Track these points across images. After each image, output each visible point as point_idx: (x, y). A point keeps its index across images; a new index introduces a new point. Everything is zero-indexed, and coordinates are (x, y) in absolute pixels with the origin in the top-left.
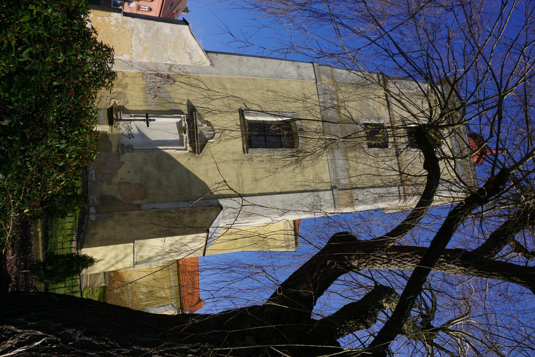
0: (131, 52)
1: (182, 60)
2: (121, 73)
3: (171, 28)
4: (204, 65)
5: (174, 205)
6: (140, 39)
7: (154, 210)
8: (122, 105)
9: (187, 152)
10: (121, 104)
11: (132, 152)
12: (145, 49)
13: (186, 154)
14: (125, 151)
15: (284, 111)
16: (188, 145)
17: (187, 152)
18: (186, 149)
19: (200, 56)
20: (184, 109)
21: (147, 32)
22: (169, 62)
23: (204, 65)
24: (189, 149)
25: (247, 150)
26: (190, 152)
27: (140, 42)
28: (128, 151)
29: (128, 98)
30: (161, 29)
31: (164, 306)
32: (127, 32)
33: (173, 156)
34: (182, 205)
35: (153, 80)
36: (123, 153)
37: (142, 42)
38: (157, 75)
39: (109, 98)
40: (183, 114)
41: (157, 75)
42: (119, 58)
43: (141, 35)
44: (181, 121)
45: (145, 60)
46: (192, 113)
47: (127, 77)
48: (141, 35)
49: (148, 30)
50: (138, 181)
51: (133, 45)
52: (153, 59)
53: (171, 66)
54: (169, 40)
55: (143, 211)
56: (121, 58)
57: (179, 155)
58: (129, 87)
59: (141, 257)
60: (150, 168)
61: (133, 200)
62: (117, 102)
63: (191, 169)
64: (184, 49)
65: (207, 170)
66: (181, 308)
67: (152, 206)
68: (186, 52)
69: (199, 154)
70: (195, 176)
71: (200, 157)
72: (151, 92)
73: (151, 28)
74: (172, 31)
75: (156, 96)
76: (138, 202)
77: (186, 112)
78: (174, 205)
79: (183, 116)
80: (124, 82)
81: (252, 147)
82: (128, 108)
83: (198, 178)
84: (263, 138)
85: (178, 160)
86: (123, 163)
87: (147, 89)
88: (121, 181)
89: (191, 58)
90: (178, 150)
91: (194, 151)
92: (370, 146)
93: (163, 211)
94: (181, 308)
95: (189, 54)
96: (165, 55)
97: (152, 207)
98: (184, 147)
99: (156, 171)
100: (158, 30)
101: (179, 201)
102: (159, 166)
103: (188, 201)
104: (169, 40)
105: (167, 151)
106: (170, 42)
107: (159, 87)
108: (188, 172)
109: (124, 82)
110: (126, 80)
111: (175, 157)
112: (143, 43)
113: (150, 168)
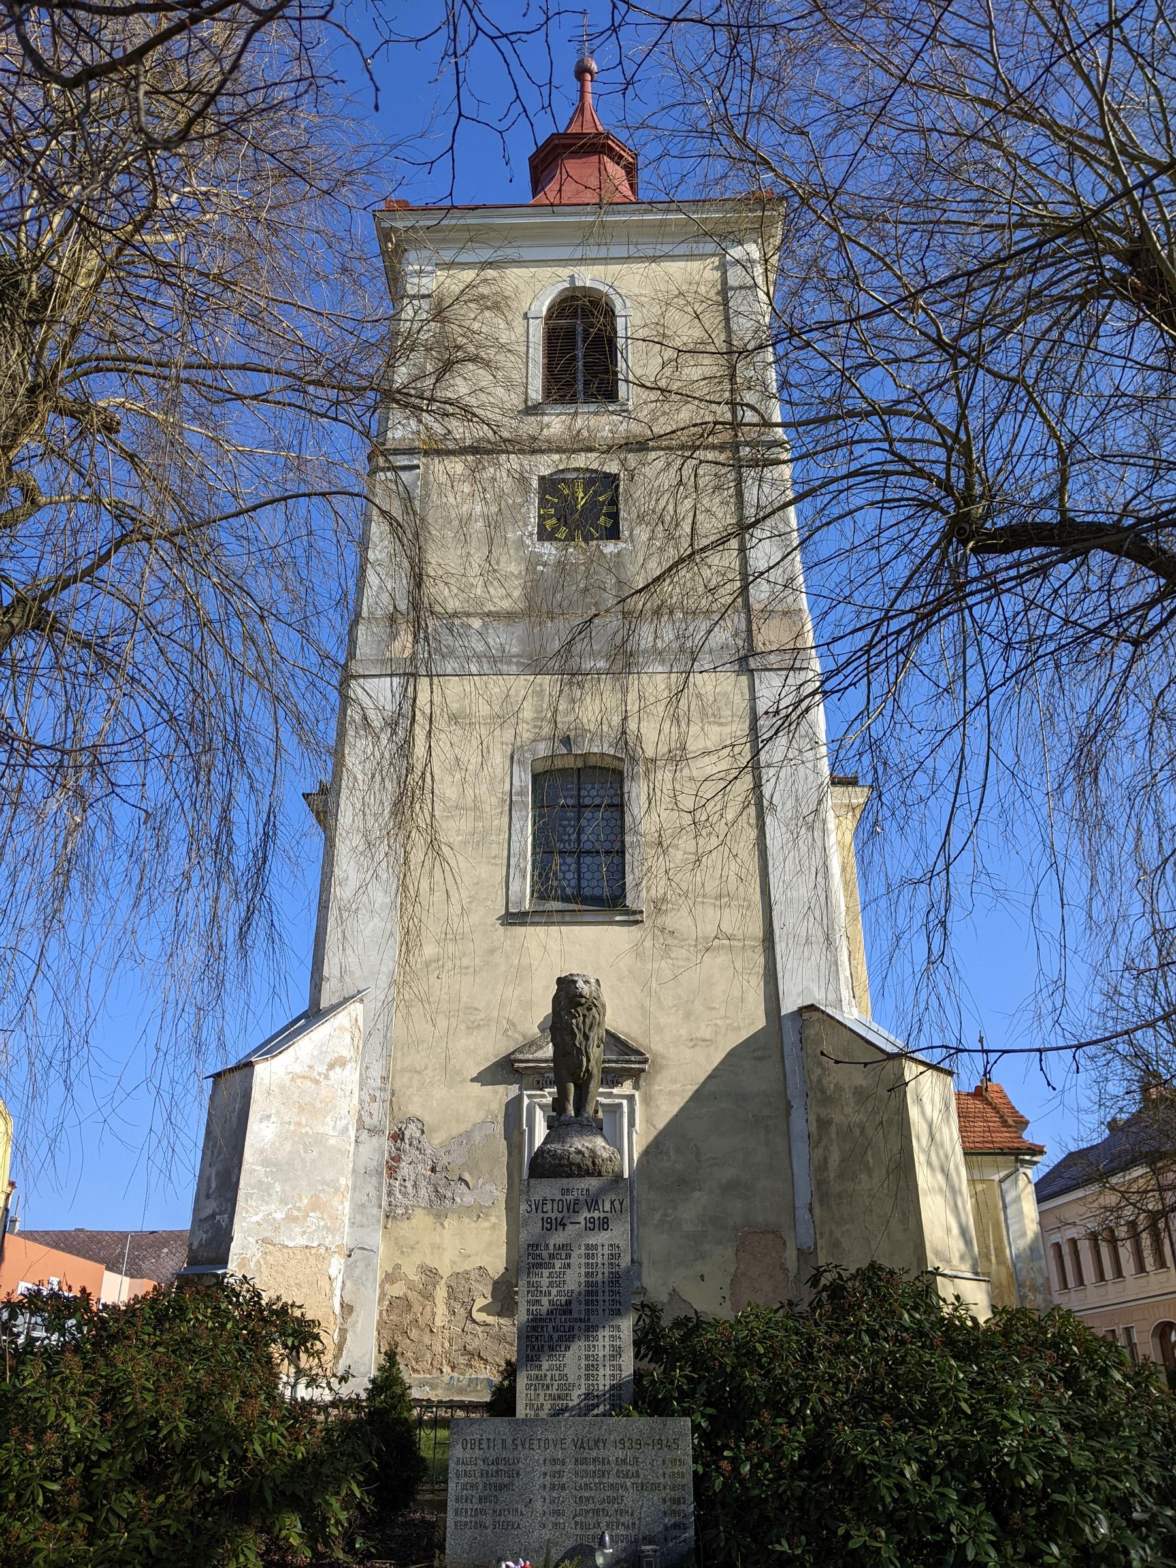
0: (322, 1250)
1: (346, 1092)
2: (387, 1286)
3: (261, 1120)
4: (361, 1023)
5: (800, 1149)
6: (290, 1218)
7: (817, 1211)
8: (490, 1288)
9: (637, 1094)
10: (488, 1290)
11: (640, 1264)
12: (315, 1206)
13: (647, 1101)
14: (637, 1284)
15: (507, 787)
16: (615, 1091)
17: (637, 1094)
18: (631, 1099)
19: (332, 1036)
20: (504, 1093)
21: (270, 1195)
22: (352, 1133)
23: (361, 1023)
24: (627, 1088)
25: (634, 913)
26: (636, 1087)
27: (295, 1219)
28: (639, 1278)
29: (467, 1266)
30: (262, 1151)
31: (1005, 1207)
32: (270, 1259)
33: (651, 1138)
34: (800, 1122)
35: (409, 1184)
36: (644, 1290)
37: (295, 1213)
38: (392, 1171)
39: (470, 1326)
40: (519, 1099)
41: (392, 1171)
42: (338, 1292)
43: (279, 1216)
44: (541, 1106)
45: (345, 1208)
46: (517, 1071)
47: (397, 1267)
48: (279, 1216)
49: (265, 1191)
50: (730, 1252)
51: (305, 1242)
52: (343, 1181)
53: (361, 1125)
54: (292, 1127)
55: (820, 1243)
56: (339, 1284)
57: (649, 1121)
58: (432, 1262)
59: (962, 1258)
60: (690, 1211)
61: (786, 1270)
62: (480, 1302)
63: (691, 1089)
64: (317, 1082)
65: (694, 1042)
66: (1017, 1155)
67: (803, 1214)
68: (327, 1077)
69: (645, 1061)
70: (710, 1077)
71: (655, 1055)
72: (449, 1194)
73: (260, 1182)
74: (269, 1117)
75: (460, 1179)
76: (791, 1254)
77: (514, 1090)
78: (800, 1149)
79: (526, 1101)
80: (416, 1278)
81: (623, 896)
82: (502, 1271)
83: (716, 1069)
84: (588, 860)
85: (661, 1124)
86: (674, 1293)
87: (439, 1204)
88: (728, 1304)
89: (341, 1062)
90: (632, 1124)
91: (635, 1075)
92: (613, 533)
93: (819, 1183)
94: (1017, 1155)
95: (331, 1067)
96: (332, 1142)
97: (807, 1216)
98: (625, 1102)
99: (697, 1194)
100: (265, 1162)
101: (788, 1134)
102: (683, 1184)
103: (789, 1106)
104: (292, 1127)
105: (636, 1158)
106: (299, 1124)
107: (433, 1170)
108: (697, 1097)
109: (416, 1278)
110: (410, 1271)
111: (654, 1133)
112: (299, 1209)
113: (690, 1211)
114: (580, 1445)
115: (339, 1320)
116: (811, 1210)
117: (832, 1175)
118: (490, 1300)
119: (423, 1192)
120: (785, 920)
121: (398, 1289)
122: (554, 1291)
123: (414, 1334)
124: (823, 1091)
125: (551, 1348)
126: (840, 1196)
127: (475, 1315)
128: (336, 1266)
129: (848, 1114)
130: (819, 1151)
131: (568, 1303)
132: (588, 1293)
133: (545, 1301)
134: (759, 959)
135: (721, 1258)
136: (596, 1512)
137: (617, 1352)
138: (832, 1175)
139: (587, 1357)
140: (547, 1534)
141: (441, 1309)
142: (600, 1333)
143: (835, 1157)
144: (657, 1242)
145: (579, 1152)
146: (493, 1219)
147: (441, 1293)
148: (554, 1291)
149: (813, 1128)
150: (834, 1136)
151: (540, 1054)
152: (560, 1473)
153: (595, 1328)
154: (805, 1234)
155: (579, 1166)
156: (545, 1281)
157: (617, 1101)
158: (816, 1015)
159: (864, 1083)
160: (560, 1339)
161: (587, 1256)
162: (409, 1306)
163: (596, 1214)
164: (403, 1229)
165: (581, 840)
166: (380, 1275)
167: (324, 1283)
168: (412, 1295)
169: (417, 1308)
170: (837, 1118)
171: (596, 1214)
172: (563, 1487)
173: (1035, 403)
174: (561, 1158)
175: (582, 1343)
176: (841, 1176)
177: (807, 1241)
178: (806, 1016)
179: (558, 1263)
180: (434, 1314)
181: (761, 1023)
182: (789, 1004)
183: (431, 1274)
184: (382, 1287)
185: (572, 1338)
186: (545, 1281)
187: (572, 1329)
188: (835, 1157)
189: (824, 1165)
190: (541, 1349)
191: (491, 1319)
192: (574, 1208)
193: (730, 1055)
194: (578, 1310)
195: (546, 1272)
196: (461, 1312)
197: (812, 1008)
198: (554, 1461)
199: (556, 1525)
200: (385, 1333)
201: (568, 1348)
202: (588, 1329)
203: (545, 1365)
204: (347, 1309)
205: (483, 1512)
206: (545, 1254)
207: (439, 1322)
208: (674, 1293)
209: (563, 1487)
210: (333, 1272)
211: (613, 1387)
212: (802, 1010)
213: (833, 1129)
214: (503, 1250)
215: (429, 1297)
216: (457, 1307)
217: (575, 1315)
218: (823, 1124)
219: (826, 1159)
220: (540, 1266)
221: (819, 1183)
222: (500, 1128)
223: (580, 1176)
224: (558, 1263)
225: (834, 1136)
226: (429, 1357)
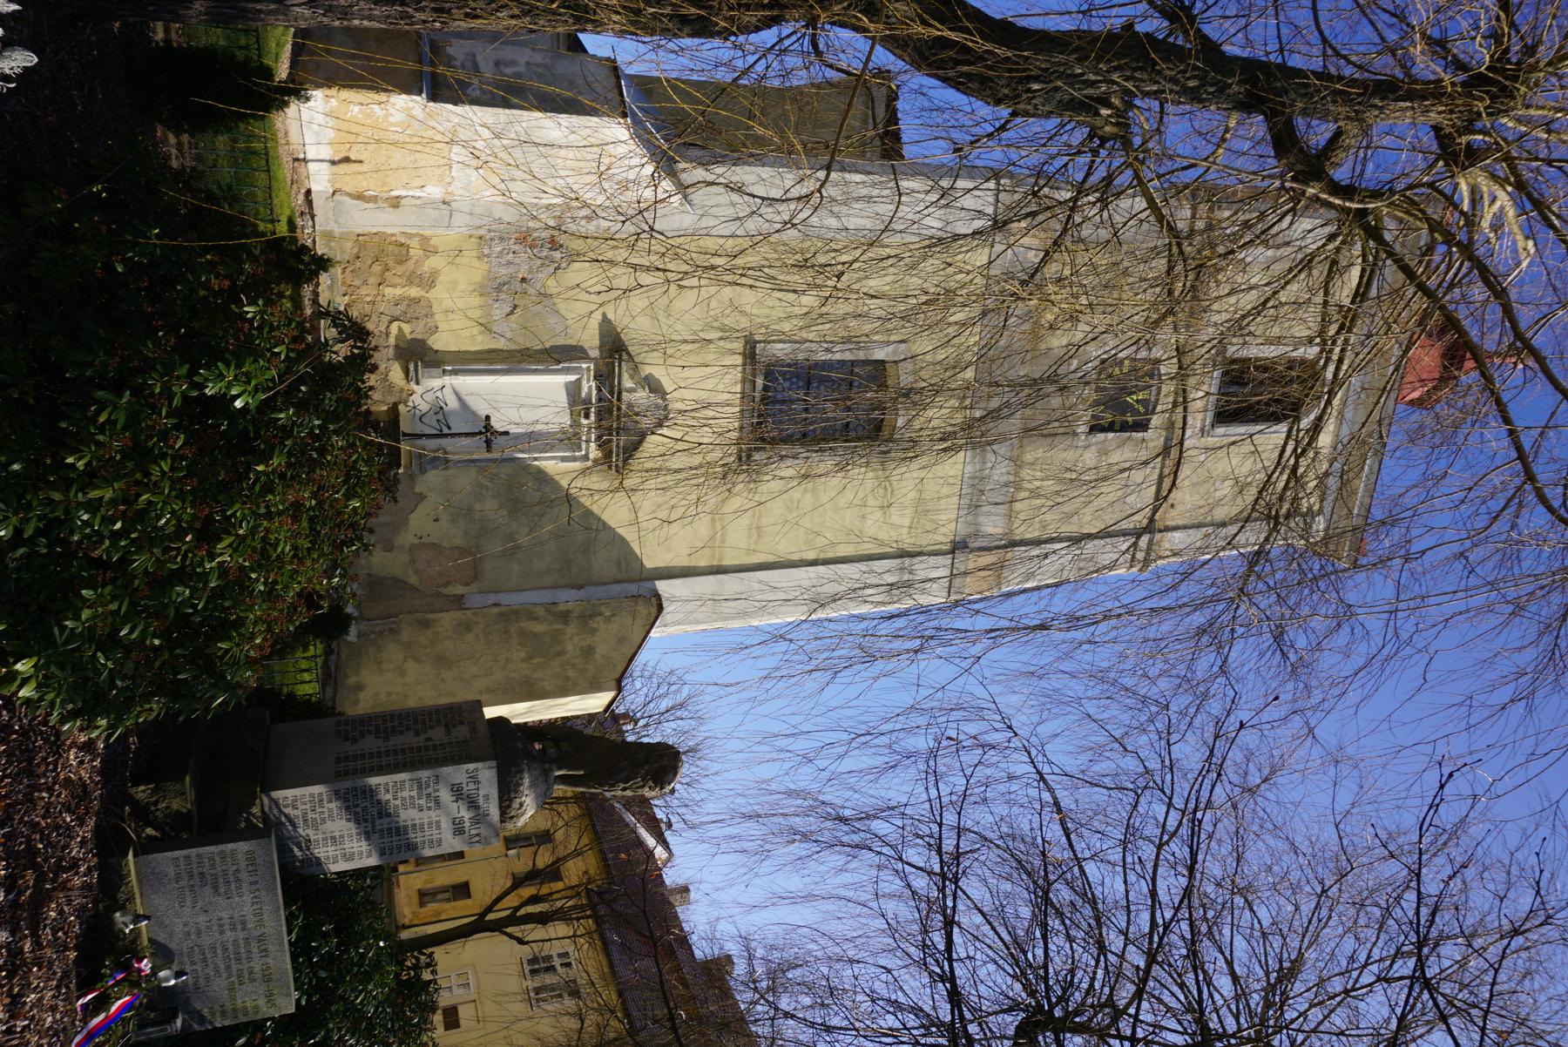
5: (544, 597)
7: (495, 610)
8: (420, 337)
20: (590, 338)
24: (594, 453)
26: (596, 461)
34: (567, 598)
39: (385, 319)
40: (586, 357)
42: (411, 193)
44: (579, 380)
50: (458, 542)
61: (446, 585)
62: (407, 328)
67: (492, 599)
75: (515, 307)
76: (459, 589)
77: (595, 353)
78: (544, 597)
80: (426, 268)
82: (435, 347)
86: (422, 497)
90: (563, 459)
102: (514, 504)
103: (580, 587)
109: (426, 268)
114: (261, 939)
115: (385, 195)
116: (495, 605)
117: (523, 625)
118: (409, 337)
119: (503, 271)
120: (731, 583)
121: (415, 253)
122: (398, 802)
123: (377, 268)
124: (592, 616)
125: (347, 808)
126: (507, 632)
127: (395, 324)
128: (435, 191)
129: (573, 641)
130: (541, 612)
131: (389, 815)
132: (398, 829)
133: (389, 796)
134: (702, 562)
135: (452, 534)
136: (205, 960)
137: (349, 857)
138: (523, 625)
139: (342, 836)
140: (179, 928)
141: (398, 291)
142: (364, 843)
143: (538, 627)
144: (464, 481)
145: (521, 805)
146: (480, 338)
147: (414, 292)
148: (398, 802)
149: (562, 607)
150: (555, 626)
151: (625, 376)
152: (234, 929)
153: (368, 838)
154: (476, 601)
155: (509, 806)
156: (406, 794)
157: (584, 446)
158: (654, 611)
159: (597, 656)
160: (356, 814)
161: (430, 823)
162: (401, 263)
163: (467, 824)
164: (469, 256)
165: (813, 407)
166: (427, 233)
167: (418, 182)
168: (410, 265)
169: (399, 270)
170: (571, 629)
171: (467, 824)
172: (222, 933)
173: (1148, 554)
174: (516, 791)
175: (354, 831)
176: (523, 633)
177: (469, 603)
178: (654, 600)
179: (423, 802)
180: (394, 286)
181: (649, 563)
182: (662, 586)
183: (429, 282)
184: (417, 235)
185: (357, 822)
186: (406, 794)
187: (366, 821)
188: (538, 627)
189: (532, 617)
190: (346, 800)
191: (392, 340)
192: (473, 804)
193: (623, 540)
194: (383, 823)
195: (414, 793)
196: (397, 311)
197: (660, 608)
198: (244, 923)
199: (188, 934)
200: (376, 239)
201: (349, 820)
202: (366, 833)
203: (333, 805)
204: (396, 203)
205: (191, 877)
206: (430, 790)
207: (388, 291)
208: (422, 497)
209: (222, 933)
210: (429, 189)
211: (318, 859)
212: (658, 596)
213: (561, 626)
214: (453, 348)
215: (410, 281)
216: (401, 308)
217: (378, 822)
218: (565, 617)
219: (535, 619)
220: (420, 787)
221: (517, 612)
222: (560, 341)
223: (501, 807)
224: (423, 802)
225: (555, 626)
226: (357, 283)
